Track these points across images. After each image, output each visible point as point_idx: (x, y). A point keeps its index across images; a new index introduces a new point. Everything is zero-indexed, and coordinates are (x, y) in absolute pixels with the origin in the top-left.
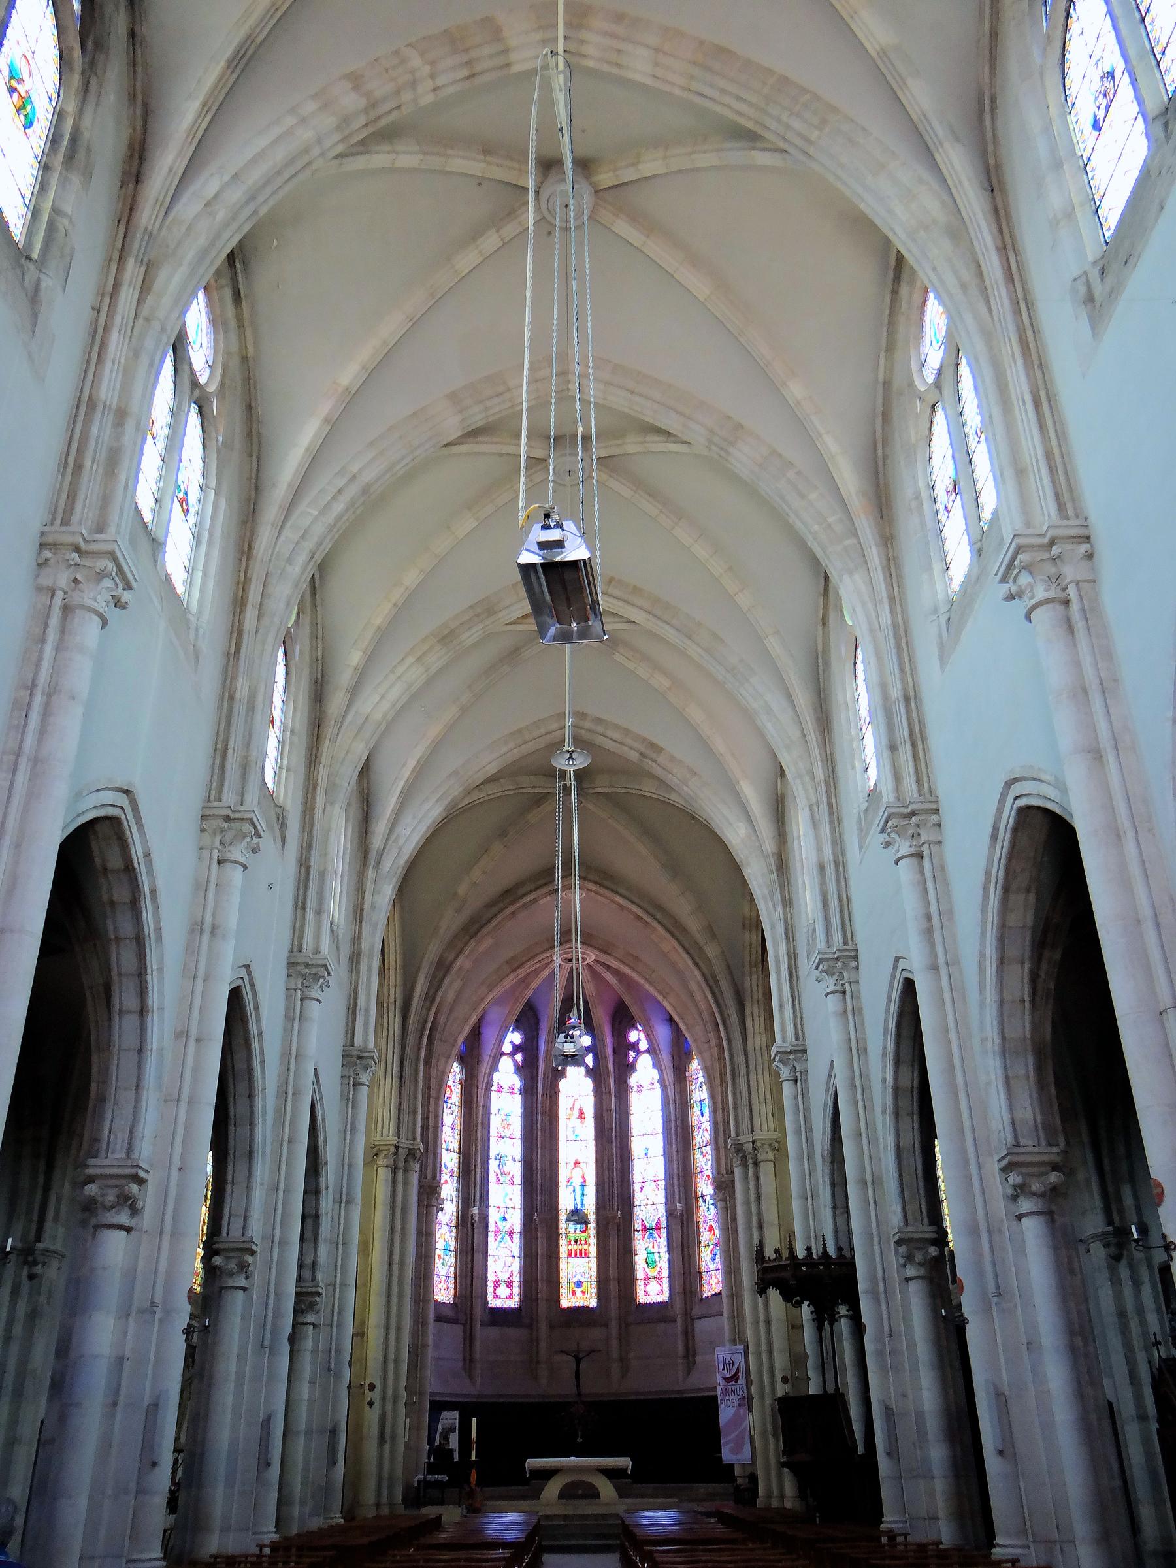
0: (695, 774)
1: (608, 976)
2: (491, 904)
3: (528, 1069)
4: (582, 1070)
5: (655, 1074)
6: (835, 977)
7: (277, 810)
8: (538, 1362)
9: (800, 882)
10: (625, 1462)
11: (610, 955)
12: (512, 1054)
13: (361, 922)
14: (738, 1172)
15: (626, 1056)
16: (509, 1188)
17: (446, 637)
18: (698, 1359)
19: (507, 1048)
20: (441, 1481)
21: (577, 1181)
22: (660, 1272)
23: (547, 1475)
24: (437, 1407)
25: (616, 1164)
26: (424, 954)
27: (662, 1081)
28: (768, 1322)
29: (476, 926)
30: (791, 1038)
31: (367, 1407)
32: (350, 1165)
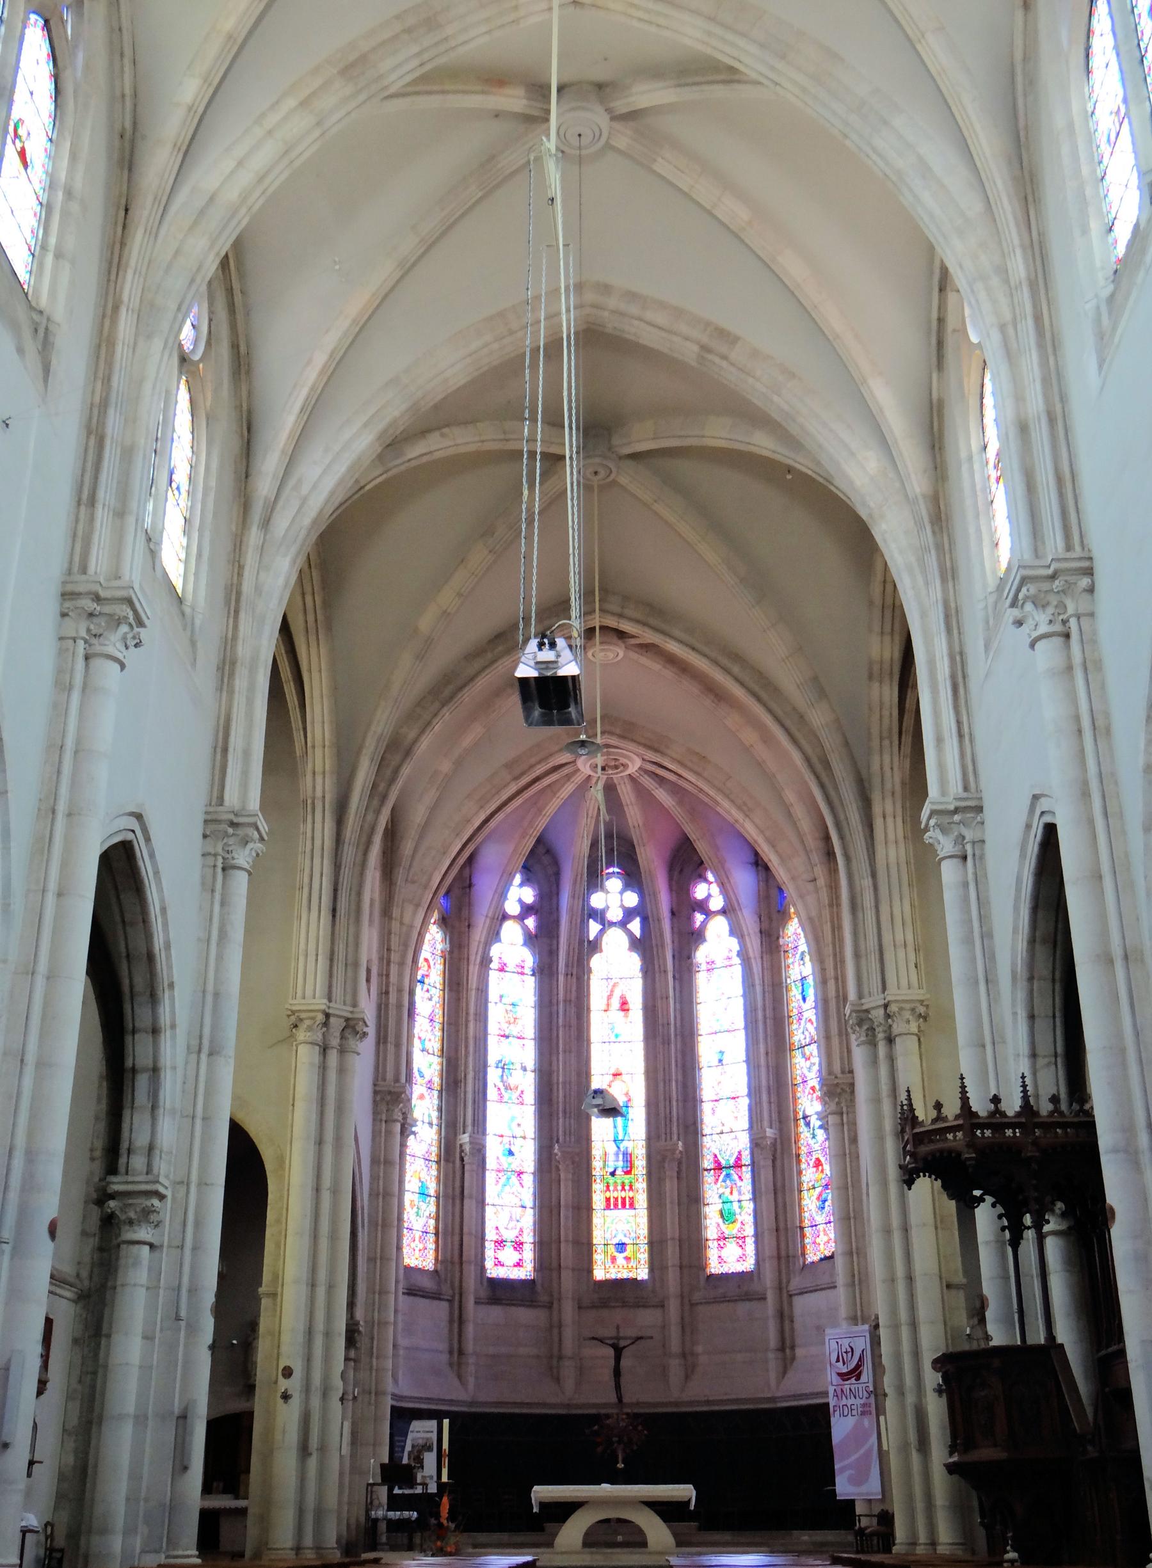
0: (793, 375)
1: (663, 796)
2: (472, 656)
3: (543, 939)
4: (624, 940)
5: (734, 944)
6: (1050, 610)
7: (35, 317)
8: (560, 1358)
9: (972, 530)
10: (685, 1491)
11: (663, 754)
12: (521, 918)
13: (237, 612)
14: (859, 1055)
15: (690, 919)
17: (353, 67)
18: (799, 1352)
19: (512, 907)
20: (408, 1521)
22: (740, 1230)
23: (563, 1511)
24: (402, 1417)
25: (675, 1074)
26: (369, 725)
27: (743, 954)
28: (910, 1279)
29: (451, 688)
30: (955, 787)
31: (280, 1401)
32: (216, 995)
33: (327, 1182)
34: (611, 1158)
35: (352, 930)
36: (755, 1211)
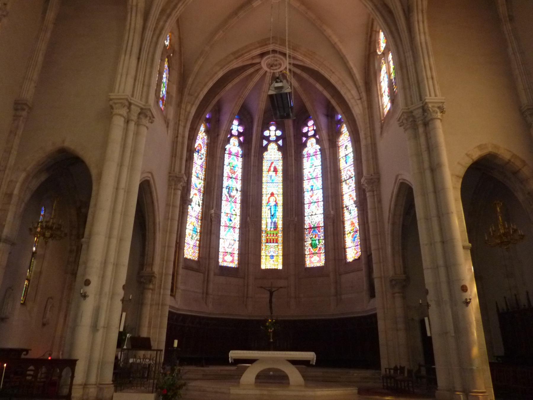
3: (245, 145)
8: (247, 297)
10: (310, 356)
16: (233, 204)
19: (235, 132)
21: (272, 203)
23: (251, 361)
33: (123, 185)
34: (269, 224)
35: (148, 70)
36: (325, 243)
